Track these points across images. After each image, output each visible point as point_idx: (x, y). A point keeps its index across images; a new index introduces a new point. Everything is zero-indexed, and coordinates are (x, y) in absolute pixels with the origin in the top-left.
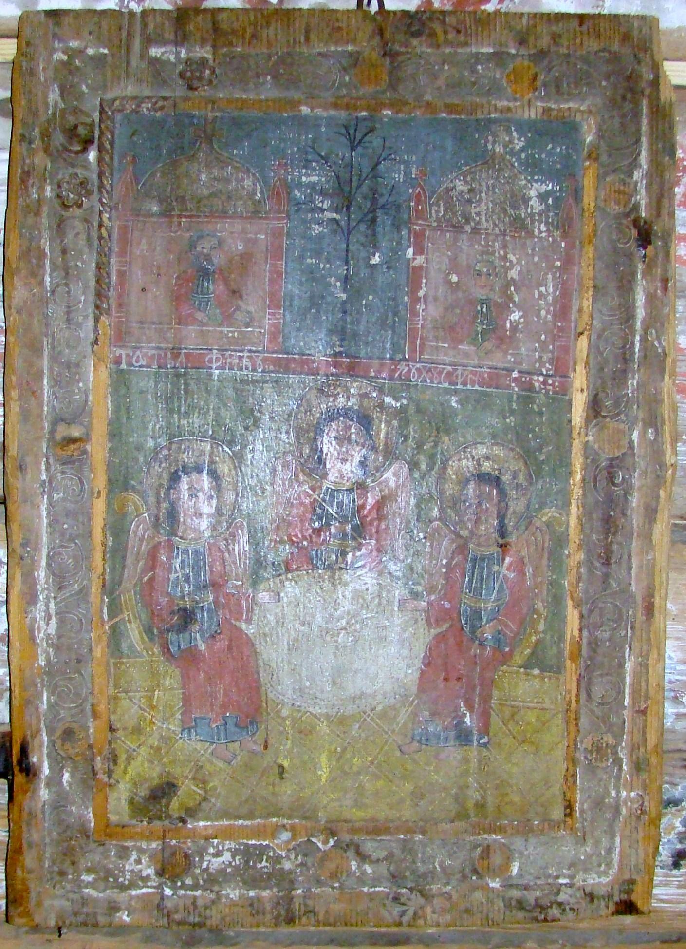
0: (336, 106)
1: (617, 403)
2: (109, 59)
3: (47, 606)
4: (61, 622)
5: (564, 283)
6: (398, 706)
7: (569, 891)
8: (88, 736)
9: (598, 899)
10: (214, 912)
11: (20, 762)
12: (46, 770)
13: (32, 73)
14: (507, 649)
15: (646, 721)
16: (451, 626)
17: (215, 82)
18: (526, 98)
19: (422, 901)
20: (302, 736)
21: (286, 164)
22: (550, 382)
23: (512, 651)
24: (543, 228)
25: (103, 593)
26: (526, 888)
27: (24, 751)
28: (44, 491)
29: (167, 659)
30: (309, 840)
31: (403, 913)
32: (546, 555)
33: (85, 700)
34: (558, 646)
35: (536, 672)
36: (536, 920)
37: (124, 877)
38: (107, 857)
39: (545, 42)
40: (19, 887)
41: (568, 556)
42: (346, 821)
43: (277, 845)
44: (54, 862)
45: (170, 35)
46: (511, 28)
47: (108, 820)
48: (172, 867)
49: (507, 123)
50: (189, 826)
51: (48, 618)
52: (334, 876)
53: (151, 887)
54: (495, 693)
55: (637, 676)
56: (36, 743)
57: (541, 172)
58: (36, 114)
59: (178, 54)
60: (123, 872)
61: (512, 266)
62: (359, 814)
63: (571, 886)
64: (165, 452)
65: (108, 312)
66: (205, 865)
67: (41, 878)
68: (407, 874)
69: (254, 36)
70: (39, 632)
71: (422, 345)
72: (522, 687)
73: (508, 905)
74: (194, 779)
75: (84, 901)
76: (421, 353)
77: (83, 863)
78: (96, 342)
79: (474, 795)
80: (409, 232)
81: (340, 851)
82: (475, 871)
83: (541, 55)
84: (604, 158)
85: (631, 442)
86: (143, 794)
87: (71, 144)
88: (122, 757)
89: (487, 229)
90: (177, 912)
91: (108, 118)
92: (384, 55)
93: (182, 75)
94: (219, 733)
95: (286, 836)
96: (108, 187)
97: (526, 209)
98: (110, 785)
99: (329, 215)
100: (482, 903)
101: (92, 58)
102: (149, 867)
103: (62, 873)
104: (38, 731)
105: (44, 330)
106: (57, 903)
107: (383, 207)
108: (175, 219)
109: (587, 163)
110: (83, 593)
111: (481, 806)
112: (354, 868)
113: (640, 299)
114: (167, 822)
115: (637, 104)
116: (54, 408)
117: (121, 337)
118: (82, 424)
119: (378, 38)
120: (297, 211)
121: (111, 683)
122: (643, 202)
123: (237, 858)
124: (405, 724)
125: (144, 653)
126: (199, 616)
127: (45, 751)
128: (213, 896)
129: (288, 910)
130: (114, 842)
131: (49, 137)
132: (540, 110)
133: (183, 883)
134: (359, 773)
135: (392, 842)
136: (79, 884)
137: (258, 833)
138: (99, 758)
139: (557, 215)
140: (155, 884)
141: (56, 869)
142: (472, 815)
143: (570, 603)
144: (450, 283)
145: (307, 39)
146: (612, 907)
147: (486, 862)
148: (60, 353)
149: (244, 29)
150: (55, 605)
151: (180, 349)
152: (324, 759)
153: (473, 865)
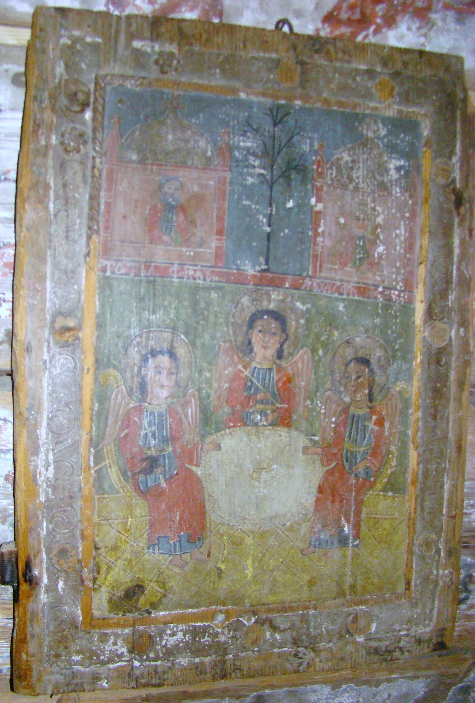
0: (264, 95)
1: (442, 312)
2: (102, 47)
3: (47, 456)
4: (57, 468)
5: (411, 228)
6: (301, 522)
7: (406, 639)
8: (78, 554)
9: (423, 642)
10: (170, 675)
11: (25, 575)
12: (45, 580)
13: (44, 51)
14: (372, 479)
15: (455, 523)
16: (337, 464)
17: (180, 69)
18: (387, 103)
19: (312, 654)
20: (235, 546)
21: (229, 133)
22: (402, 295)
23: (375, 480)
24: (398, 190)
25: (91, 445)
26: (380, 639)
27: (28, 566)
28: (46, 368)
29: (139, 495)
30: (238, 620)
31: (301, 664)
32: (398, 414)
33: (76, 526)
34: (404, 477)
35: (390, 494)
36: (386, 660)
37: (104, 655)
38: (92, 642)
39: (399, 66)
40: (24, 667)
41: (412, 414)
42: (263, 604)
43: (216, 625)
44: (51, 648)
45: (147, 34)
46: (377, 55)
47: (92, 614)
48: (138, 646)
49: (375, 118)
50: (153, 615)
51: (47, 466)
52: (255, 642)
53: (124, 661)
54: (364, 510)
55: (451, 493)
56: (38, 560)
57: (397, 152)
58: (45, 81)
59: (153, 47)
60: (103, 652)
61: (378, 216)
62: (272, 598)
63: (407, 635)
64: (138, 339)
65: (97, 232)
66: (164, 643)
67: (41, 660)
68: (304, 637)
69: (207, 41)
70: (40, 476)
71: (321, 266)
72: (380, 504)
73: (368, 653)
74: (156, 581)
75: (74, 675)
76: (320, 271)
77: (74, 647)
78: (88, 254)
79: (349, 581)
80: (313, 187)
81: (259, 625)
82: (348, 632)
83: (397, 74)
84: (435, 146)
85: (451, 337)
86: (119, 594)
87: (72, 106)
88: (104, 568)
89: (363, 188)
90: (143, 677)
91: (101, 88)
92: (297, 62)
93: (157, 62)
94: (175, 548)
95: (221, 617)
96: (100, 139)
97: (388, 175)
98: (94, 589)
99: (259, 171)
100: (352, 652)
101: (90, 45)
102: (123, 647)
103: (58, 656)
104: (39, 551)
105: (48, 244)
106: (53, 677)
107: (295, 168)
108: (149, 167)
109: (425, 149)
110: (75, 445)
111: (353, 587)
112: (268, 636)
113: (456, 241)
114: (137, 614)
115: (453, 113)
116: (54, 304)
117: (106, 251)
118: (76, 317)
119: (292, 52)
120: (237, 166)
121: (96, 514)
122: (458, 178)
123: (187, 636)
124: (305, 535)
125: (121, 490)
126: (161, 461)
127: (45, 566)
128: (169, 664)
129: (223, 669)
130: (97, 631)
131: (55, 99)
132: (396, 112)
133: (148, 656)
134: (273, 571)
135: (294, 616)
136: (70, 663)
137: (203, 617)
138: (86, 570)
139: (406, 182)
140: (127, 659)
141: (53, 653)
142: (347, 593)
143: (411, 446)
144: (338, 223)
145: (245, 47)
146: (431, 646)
147: (355, 625)
148: (59, 262)
149: (201, 36)
150: (54, 455)
151: (151, 262)
152: (249, 562)
153: (347, 627)
